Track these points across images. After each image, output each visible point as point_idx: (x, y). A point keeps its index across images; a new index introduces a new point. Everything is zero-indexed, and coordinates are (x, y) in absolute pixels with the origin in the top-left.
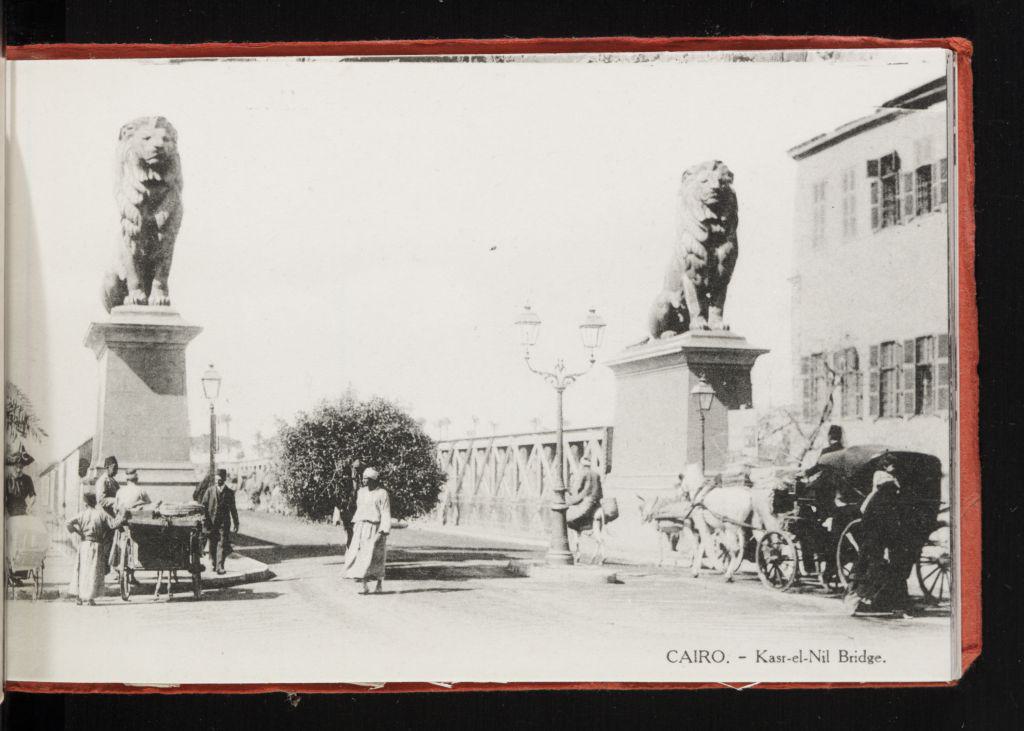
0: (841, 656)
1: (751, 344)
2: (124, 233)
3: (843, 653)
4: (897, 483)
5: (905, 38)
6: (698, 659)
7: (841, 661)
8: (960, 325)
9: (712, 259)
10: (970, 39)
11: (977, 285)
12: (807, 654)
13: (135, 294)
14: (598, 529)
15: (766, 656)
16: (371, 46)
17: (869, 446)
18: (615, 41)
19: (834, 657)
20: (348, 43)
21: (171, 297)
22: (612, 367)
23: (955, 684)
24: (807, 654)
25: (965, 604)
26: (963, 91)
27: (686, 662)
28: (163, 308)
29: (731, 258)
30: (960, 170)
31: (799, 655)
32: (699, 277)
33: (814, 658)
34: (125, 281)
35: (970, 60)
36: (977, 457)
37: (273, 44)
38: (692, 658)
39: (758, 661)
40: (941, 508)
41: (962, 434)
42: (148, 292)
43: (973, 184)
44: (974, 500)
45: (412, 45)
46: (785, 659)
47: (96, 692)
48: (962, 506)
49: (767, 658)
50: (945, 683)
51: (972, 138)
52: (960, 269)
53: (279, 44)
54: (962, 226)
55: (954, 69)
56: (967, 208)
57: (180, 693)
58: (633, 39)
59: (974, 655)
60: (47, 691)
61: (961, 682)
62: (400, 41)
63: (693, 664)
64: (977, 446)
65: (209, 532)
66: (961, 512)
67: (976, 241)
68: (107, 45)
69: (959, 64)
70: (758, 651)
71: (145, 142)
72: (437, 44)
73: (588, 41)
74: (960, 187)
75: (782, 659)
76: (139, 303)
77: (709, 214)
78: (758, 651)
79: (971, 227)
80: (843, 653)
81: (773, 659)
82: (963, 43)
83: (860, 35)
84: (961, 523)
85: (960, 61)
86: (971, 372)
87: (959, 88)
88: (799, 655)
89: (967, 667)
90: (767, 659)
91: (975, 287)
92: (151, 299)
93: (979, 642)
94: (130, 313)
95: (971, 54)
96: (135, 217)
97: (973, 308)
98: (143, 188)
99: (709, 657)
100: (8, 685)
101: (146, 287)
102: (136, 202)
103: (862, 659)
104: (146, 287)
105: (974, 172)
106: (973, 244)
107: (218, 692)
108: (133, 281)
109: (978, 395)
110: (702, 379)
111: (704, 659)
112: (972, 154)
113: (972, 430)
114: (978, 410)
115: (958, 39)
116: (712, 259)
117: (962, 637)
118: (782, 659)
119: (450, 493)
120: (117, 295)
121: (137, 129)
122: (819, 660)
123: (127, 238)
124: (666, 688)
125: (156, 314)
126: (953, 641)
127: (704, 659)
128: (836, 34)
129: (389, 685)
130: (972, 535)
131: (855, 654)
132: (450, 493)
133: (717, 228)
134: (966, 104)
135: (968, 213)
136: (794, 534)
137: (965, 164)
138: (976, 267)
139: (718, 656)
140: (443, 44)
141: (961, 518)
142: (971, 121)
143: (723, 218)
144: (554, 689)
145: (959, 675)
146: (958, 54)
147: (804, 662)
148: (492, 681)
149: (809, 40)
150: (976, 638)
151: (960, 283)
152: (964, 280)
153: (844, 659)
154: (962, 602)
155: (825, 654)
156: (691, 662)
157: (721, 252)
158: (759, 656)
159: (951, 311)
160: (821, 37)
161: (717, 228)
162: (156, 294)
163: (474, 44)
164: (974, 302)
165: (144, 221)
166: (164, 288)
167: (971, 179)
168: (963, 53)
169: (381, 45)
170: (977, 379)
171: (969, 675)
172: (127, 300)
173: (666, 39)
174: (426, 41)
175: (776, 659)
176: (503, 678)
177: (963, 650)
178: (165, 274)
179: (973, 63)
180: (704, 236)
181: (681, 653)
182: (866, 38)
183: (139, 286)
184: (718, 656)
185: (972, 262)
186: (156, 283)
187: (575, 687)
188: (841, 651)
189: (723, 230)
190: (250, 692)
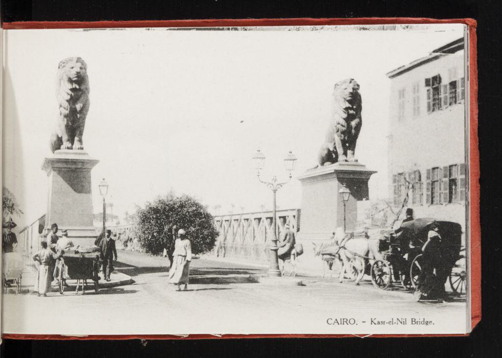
0: (412, 321)
1: (368, 168)
2: (61, 114)
3: (414, 320)
4: (440, 237)
5: (444, 19)
6: (342, 323)
7: (412, 324)
8: (471, 159)
9: (349, 127)
10: (475, 19)
11: (479, 140)
12: (396, 320)
13: (66, 144)
14: (293, 259)
15: (376, 321)
16: (182, 22)
17: (426, 218)
18: (302, 20)
19: (409, 322)
20: (170, 21)
21: (84, 145)
22: (300, 180)
23: (468, 335)
24: (396, 320)
25: (473, 296)
26: (472, 44)
27: (336, 324)
28: (80, 151)
29: (358, 127)
30: (470, 83)
31: (391, 321)
32: (342, 135)
33: (399, 322)
34: (62, 137)
35: (476, 30)
36: (479, 224)
37: (134, 22)
38: (339, 322)
39: (372, 324)
40: (461, 249)
41: (472, 212)
42: (72, 143)
43: (477, 90)
44: (478, 245)
45: (202, 22)
46: (385, 323)
47: (47, 339)
48: (471, 248)
49: (376, 322)
50: (463, 334)
51: (476, 67)
52: (471, 132)
53: (137, 21)
54: (472, 111)
55: (468, 34)
56: (474, 102)
57: (88, 339)
58: (310, 19)
59: (478, 321)
60: (23, 338)
61: (471, 334)
62: (196, 20)
63: (340, 325)
64: (479, 219)
65: (102, 261)
66: (471, 251)
67: (479, 118)
68: (52, 22)
69: (470, 32)
70: (372, 319)
71: (71, 70)
72: (214, 22)
73: (288, 20)
74: (470, 92)
75: (383, 323)
76: (68, 148)
77: (348, 105)
78: (372, 319)
79: (476, 111)
80: (414, 320)
81: (379, 323)
82: (472, 21)
83: (422, 17)
84: (471, 256)
85: (471, 30)
86: (476, 182)
87: (470, 43)
88: (391, 321)
89: (474, 326)
90: (376, 323)
91: (478, 141)
92: (74, 147)
93: (480, 315)
94: (64, 153)
95: (476, 27)
96: (66, 106)
97: (477, 151)
98: (70, 92)
99: (348, 322)
100: (4, 335)
101: (72, 140)
102: (67, 99)
103: (423, 323)
104: (72, 140)
105: (477, 84)
106: (477, 120)
107: (107, 339)
108: (65, 138)
109: (479, 194)
110: (344, 186)
111: (345, 323)
112: (476, 76)
113: (476, 211)
114: (479, 201)
115: (470, 19)
116: (349, 127)
117: (472, 312)
118: (383, 323)
119: (221, 242)
120: (58, 144)
121: (67, 63)
122: (401, 323)
123: (62, 116)
124: (326, 337)
125: (76, 154)
126: (467, 314)
127: (345, 323)
128: (410, 17)
129: (191, 336)
130: (476, 262)
131: (419, 320)
132: (221, 242)
133: (351, 112)
134: (474, 51)
135: (475, 104)
136: (389, 261)
137: (473, 81)
138: (479, 131)
139: (352, 321)
140: (217, 21)
141: (471, 254)
142: (476, 59)
143: (355, 107)
144: (272, 337)
145: (470, 331)
146: (470, 27)
147: (394, 324)
148: (241, 333)
149: (396, 20)
150: (479, 312)
151: (471, 138)
152: (472, 137)
153: (414, 323)
154: (472, 295)
155: (405, 320)
156: (339, 324)
157: (353, 123)
158: (372, 321)
159: (466, 152)
160: (403, 18)
161: (351, 112)
162: (76, 144)
163: (232, 22)
164: (478, 148)
165: (71, 108)
166: (80, 141)
167: (476, 88)
168: (472, 26)
169: (187, 22)
170: (479, 185)
171: (475, 331)
172: (62, 147)
173: (326, 19)
174: (209, 20)
175: (380, 323)
176: (246, 332)
177: (472, 318)
178: (81, 134)
179: (477, 31)
180: (345, 116)
181: (334, 320)
182: (424, 18)
183: (68, 140)
184: (352, 321)
185: (477, 128)
186: (76, 138)
187: (282, 337)
188: (412, 319)
189: (354, 113)
190: (123, 339)
